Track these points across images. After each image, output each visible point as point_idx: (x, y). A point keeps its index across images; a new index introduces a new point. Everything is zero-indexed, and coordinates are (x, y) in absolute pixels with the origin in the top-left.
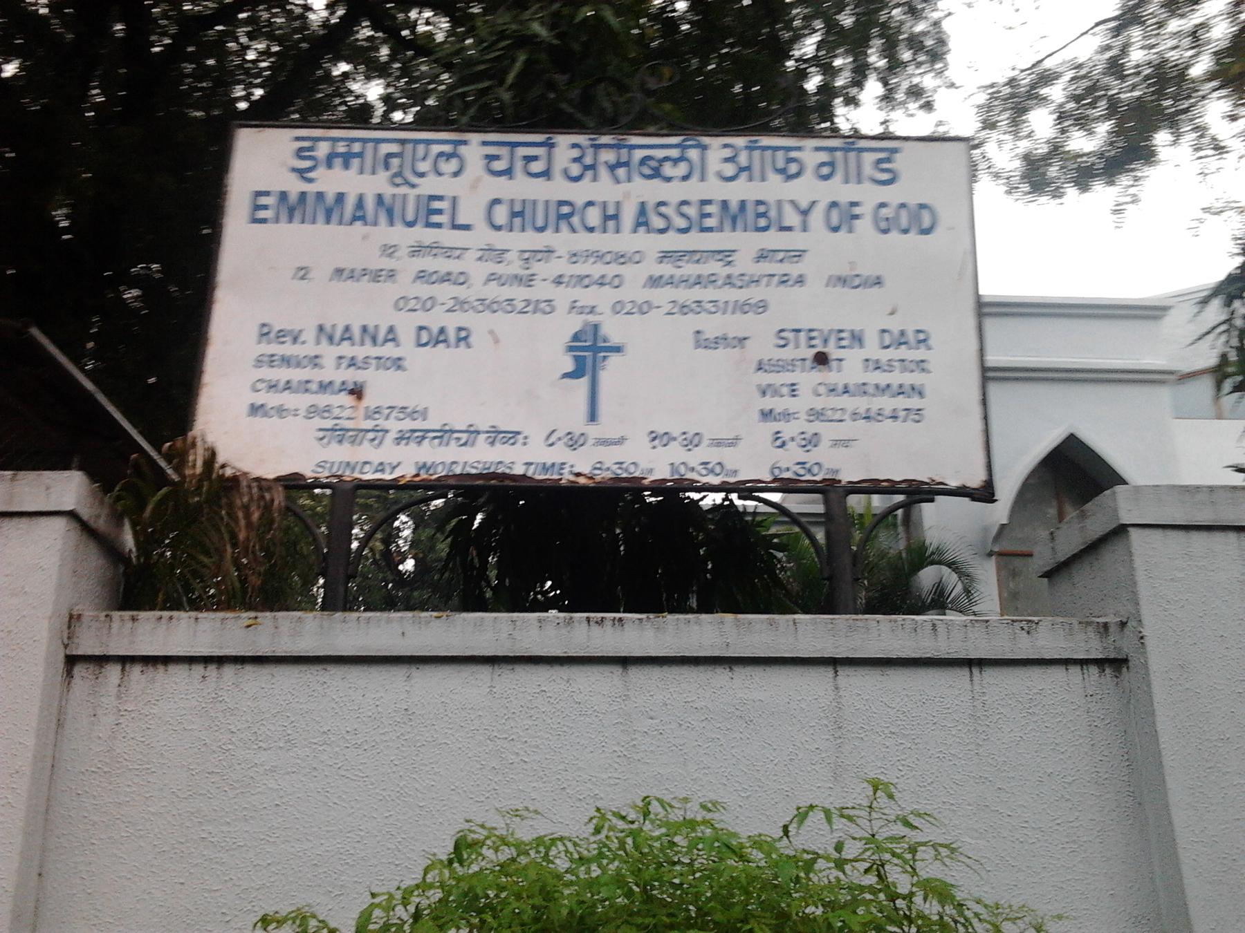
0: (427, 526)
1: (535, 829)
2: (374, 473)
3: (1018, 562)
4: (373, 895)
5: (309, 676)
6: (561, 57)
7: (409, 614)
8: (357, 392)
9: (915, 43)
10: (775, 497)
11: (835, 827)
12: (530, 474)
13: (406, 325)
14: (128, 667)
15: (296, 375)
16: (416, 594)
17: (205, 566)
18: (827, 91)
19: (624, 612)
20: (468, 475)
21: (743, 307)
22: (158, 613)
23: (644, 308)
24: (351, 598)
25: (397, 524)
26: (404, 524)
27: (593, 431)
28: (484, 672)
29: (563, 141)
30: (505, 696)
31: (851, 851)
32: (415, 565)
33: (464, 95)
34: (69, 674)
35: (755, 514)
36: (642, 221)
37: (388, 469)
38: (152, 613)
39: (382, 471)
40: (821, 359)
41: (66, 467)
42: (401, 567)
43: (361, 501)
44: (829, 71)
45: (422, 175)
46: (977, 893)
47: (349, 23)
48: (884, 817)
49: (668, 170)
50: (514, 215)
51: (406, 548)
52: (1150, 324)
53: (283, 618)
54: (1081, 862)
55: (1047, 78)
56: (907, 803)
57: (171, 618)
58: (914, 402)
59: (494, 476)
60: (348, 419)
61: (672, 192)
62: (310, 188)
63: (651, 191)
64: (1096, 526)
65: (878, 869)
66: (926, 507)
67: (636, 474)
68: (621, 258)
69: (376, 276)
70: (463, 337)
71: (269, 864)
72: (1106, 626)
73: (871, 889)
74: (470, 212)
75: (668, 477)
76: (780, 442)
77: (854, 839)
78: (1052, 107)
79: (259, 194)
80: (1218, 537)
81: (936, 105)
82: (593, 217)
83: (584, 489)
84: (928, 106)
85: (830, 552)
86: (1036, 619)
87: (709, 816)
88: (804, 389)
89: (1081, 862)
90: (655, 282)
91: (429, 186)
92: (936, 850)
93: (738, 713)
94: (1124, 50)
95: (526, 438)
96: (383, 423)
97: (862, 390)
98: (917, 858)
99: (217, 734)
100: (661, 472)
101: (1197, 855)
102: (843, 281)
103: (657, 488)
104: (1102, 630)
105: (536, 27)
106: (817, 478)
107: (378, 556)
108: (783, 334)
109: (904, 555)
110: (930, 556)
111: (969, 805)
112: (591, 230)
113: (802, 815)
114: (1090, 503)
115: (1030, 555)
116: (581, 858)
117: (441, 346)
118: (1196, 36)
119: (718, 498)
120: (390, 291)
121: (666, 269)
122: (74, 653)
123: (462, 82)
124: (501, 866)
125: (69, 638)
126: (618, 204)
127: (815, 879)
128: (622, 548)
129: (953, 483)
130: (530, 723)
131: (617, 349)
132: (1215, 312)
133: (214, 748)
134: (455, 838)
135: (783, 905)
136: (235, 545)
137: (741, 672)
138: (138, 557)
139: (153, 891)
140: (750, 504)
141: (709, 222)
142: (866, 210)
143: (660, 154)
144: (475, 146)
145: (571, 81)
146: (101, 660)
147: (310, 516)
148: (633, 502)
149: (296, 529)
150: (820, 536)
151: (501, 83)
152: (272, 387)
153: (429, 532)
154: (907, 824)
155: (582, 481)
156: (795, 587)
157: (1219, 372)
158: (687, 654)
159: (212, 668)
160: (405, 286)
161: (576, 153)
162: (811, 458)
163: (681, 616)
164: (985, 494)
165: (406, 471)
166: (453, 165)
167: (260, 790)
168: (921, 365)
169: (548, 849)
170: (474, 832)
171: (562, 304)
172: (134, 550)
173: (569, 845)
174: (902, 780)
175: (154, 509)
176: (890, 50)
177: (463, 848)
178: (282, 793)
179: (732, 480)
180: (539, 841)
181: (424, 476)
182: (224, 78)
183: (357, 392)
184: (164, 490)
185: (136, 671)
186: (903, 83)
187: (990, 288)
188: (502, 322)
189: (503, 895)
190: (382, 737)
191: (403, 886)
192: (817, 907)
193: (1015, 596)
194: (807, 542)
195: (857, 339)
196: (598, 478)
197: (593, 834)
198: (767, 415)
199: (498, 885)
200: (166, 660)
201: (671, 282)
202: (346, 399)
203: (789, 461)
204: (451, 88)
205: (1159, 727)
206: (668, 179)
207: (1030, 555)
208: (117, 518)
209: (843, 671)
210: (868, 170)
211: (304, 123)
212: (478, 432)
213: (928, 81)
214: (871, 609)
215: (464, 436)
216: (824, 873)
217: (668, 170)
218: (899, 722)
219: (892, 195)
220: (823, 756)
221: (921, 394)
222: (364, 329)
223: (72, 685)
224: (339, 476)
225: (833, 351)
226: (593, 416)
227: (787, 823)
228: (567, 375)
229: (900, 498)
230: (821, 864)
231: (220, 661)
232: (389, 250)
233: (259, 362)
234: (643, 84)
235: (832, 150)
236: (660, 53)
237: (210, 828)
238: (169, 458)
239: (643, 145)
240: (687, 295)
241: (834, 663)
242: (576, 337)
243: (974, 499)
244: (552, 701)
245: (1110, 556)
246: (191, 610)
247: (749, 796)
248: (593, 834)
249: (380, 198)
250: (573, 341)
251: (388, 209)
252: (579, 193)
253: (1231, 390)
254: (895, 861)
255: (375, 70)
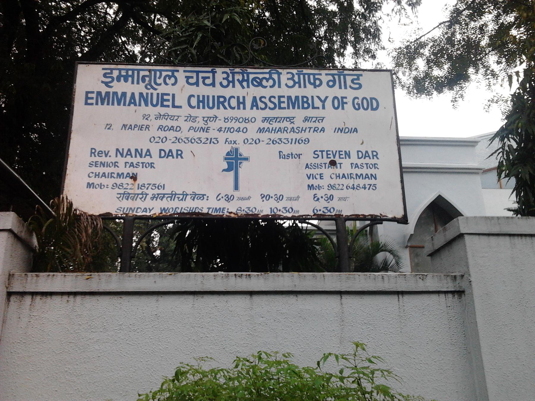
0: (166, 236)
1: (212, 366)
2: (142, 212)
3: (418, 250)
4: (139, 395)
5: (114, 300)
6: (217, 35)
7: (158, 273)
8: (134, 178)
9: (366, 31)
10: (315, 222)
11: (340, 364)
12: (210, 212)
13: (155, 149)
14: (34, 297)
15: (107, 170)
16: (161, 265)
17: (68, 253)
18: (330, 50)
19: (251, 272)
20: (184, 213)
21: (298, 141)
22: (48, 273)
23: (257, 142)
24: (133, 267)
25: (152, 235)
26: (156, 235)
27: (236, 194)
28: (190, 298)
29: (219, 71)
30: (199, 308)
31: (346, 374)
32: (161, 253)
33: (175, 51)
34: (8, 300)
35: (306, 230)
36: (254, 104)
37: (148, 211)
38: (46, 273)
39: (146, 212)
40: (333, 163)
41: (8, 210)
42: (154, 254)
43: (137, 225)
44: (331, 42)
45: (160, 84)
46: (399, 391)
47: (125, 20)
48: (361, 359)
49: (264, 83)
50: (199, 102)
51: (157, 245)
52: (470, 149)
53: (102, 275)
54: (444, 378)
55: (422, 45)
56: (370, 353)
57: (54, 275)
58: (373, 182)
59: (195, 213)
60: (130, 189)
61: (267, 92)
62: (111, 90)
63: (258, 92)
64: (450, 234)
65: (358, 381)
66: (379, 226)
67: (256, 213)
68: (246, 120)
69: (141, 128)
70: (180, 154)
71: (95, 382)
72: (455, 277)
73: (354, 390)
74: (180, 100)
75: (269, 214)
76: (316, 198)
77: (347, 367)
78: (425, 58)
79: (87, 93)
80: (501, 238)
81: (377, 56)
82: (234, 102)
83: (234, 219)
84: (374, 57)
85: (338, 247)
86: (426, 274)
87: (286, 359)
88: (326, 176)
89: (444, 378)
90: (261, 130)
91: (162, 89)
92: (383, 373)
93: (299, 315)
94: (453, 34)
95: (208, 197)
96: (145, 190)
97: (350, 176)
98: (374, 376)
99: (73, 326)
100: (266, 212)
101: (492, 374)
102: (341, 130)
103: (265, 218)
104: (453, 278)
105: (206, 22)
106: (333, 214)
107: (144, 249)
108: (316, 153)
109: (370, 248)
110: (381, 248)
111: (397, 354)
112: (234, 108)
113: (326, 357)
114: (448, 224)
115: (423, 247)
116: (230, 378)
117: (170, 158)
118: (481, 29)
119: (291, 222)
120: (146, 134)
121: (266, 125)
122: (11, 291)
123: (175, 45)
124: (196, 382)
125: (8, 284)
126: (244, 97)
127: (331, 386)
128: (250, 244)
129: (390, 216)
130: (210, 320)
131: (246, 159)
132: (497, 144)
133: (72, 332)
134: (176, 370)
135: (317, 397)
136: (81, 245)
137: (301, 298)
138: (39, 250)
139: (43, 394)
140: (305, 225)
141: (283, 105)
142: (349, 100)
143: (261, 76)
144: (181, 73)
145: (222, 45)
146: (23, 294)
147: (114, 232)
148: (254, 225)
149: (108, 237)
150: (335, 239)
151: (192, 46)
152: (97, 175)
153: (166, 238)
154: (370, 361)
155: (232, 215)
156: (324, 261)
157: (499, 169)
158: (278, 290)
159: (71, 298)
160: (154, 132)
161: (225, 76)
162: (330, 205)
163: (276, 274)
164: (404, 220)
165: (156, 211)
166: (173, 80)
167: (92, 350)
168: (375, 166)
169: (216, 374)
170: (184, 368)
171: (222, 140)
172: (37, 246)
173: (226, 373)
174: (369, 343)
175: (46, 229)
176: (356, 34)
177: (179, 374)
178: (101, 351)
179: (297, 215)
180: (212, 371)
181: (164, 213)
182: (71, 43)
183: (134, 178)
184: (51, 220)
185: (38, 298)
186: (361, 47)
187: (402, 134)
188: (195, 147)
189: (197, 394)
190: (145, 327)
191: (153, 391)
192: (332, 398)
193: (417, 265)
194: (329, 242)
195: (348, 155)
196: (239, 215)
197: (234, 368)
198: (310, 187)
199: (194, 390)
200: (51, 294)
201: (268, 130)
202: (130, 181)
203: (321, 206)
204: (170, 48)
205: (478, 320)
206: (266, 87)
207: (423, 247)
208: (30, 232)
209: (344, 297)
210: (349, 83)
211: (107, 62)
212: (187, 195)
213: (373, 47)
214: (356, 270)
215: (181, 197)
216: (335, 383)
217: (264, 83)
218: (368, 319)
219: (360, 94)
220: (336, 333)
221: (375, 178)
222: (136, 150)
223: (10, 305)
224: (127, 214)
225: (337, 159)
226: (236, 188)
227: (319, 360)
228: (224, 170)
229: (368, 222)
230: (333, 379)
231: (75, 294)
232: (146, 117)
233: (91, 165)
234: (252, 46)
235: (333, 75)
236: (260, 34)
237: (69, 366)
238: (52, 207)
239: (253, 73)
240: (274, 136)
241: (340, 293)
242: (228, 154)
243: (398, 223)
244: (219, 310)
245: (456, 247)
246: (62, 272)
247: (303, 351)
248: (234, 368)
249: (141, 94)
250: (226, 156)
251: (145, 99)
252: (227, 92)
253: (504, 176)
254: (365, 377)
255: (137, 40)
